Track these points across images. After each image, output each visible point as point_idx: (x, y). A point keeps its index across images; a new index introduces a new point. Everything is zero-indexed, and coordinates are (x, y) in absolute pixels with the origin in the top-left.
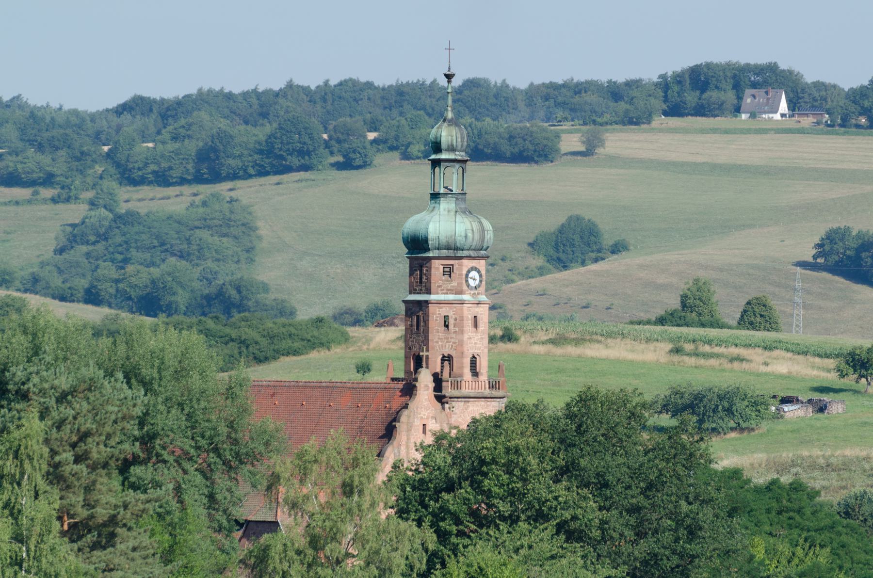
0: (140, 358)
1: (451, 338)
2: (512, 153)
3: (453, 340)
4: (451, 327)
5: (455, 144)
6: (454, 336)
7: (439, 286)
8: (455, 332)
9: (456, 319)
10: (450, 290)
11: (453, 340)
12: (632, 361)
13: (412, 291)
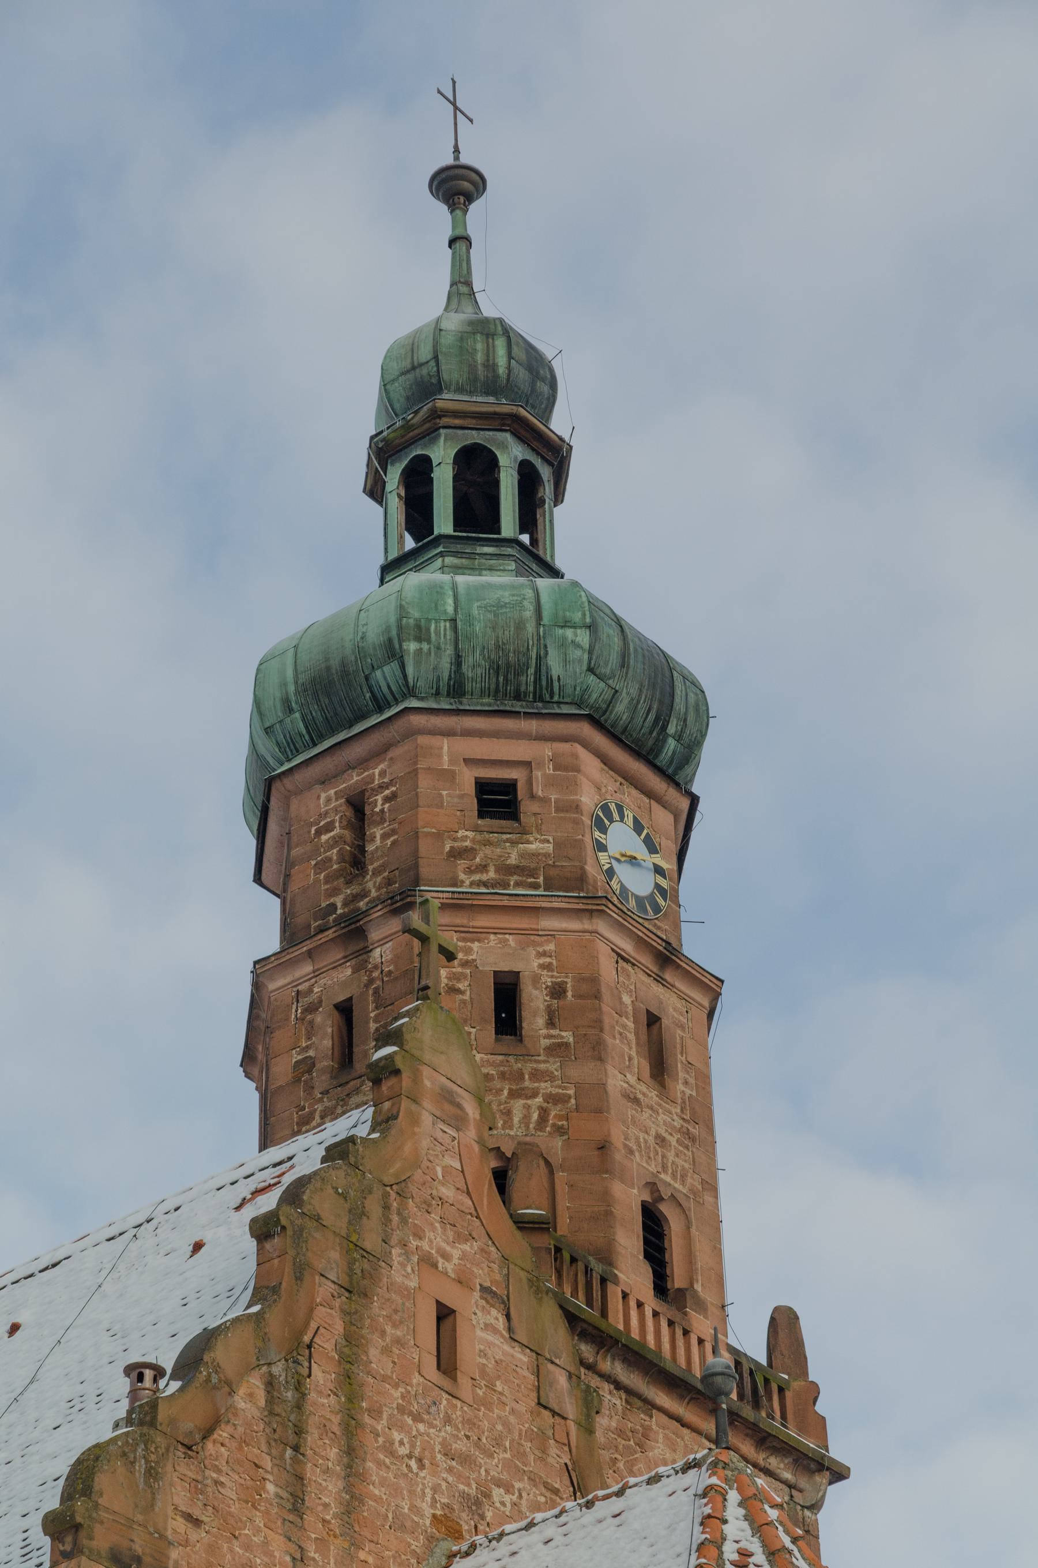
1: (536, 1075)
5: (502, 371)
6: (553, 1066)
7: (456, 854)
8: (558, 1049)
9: (557, 991)
10: (517, 870)
11: (545, 1087)
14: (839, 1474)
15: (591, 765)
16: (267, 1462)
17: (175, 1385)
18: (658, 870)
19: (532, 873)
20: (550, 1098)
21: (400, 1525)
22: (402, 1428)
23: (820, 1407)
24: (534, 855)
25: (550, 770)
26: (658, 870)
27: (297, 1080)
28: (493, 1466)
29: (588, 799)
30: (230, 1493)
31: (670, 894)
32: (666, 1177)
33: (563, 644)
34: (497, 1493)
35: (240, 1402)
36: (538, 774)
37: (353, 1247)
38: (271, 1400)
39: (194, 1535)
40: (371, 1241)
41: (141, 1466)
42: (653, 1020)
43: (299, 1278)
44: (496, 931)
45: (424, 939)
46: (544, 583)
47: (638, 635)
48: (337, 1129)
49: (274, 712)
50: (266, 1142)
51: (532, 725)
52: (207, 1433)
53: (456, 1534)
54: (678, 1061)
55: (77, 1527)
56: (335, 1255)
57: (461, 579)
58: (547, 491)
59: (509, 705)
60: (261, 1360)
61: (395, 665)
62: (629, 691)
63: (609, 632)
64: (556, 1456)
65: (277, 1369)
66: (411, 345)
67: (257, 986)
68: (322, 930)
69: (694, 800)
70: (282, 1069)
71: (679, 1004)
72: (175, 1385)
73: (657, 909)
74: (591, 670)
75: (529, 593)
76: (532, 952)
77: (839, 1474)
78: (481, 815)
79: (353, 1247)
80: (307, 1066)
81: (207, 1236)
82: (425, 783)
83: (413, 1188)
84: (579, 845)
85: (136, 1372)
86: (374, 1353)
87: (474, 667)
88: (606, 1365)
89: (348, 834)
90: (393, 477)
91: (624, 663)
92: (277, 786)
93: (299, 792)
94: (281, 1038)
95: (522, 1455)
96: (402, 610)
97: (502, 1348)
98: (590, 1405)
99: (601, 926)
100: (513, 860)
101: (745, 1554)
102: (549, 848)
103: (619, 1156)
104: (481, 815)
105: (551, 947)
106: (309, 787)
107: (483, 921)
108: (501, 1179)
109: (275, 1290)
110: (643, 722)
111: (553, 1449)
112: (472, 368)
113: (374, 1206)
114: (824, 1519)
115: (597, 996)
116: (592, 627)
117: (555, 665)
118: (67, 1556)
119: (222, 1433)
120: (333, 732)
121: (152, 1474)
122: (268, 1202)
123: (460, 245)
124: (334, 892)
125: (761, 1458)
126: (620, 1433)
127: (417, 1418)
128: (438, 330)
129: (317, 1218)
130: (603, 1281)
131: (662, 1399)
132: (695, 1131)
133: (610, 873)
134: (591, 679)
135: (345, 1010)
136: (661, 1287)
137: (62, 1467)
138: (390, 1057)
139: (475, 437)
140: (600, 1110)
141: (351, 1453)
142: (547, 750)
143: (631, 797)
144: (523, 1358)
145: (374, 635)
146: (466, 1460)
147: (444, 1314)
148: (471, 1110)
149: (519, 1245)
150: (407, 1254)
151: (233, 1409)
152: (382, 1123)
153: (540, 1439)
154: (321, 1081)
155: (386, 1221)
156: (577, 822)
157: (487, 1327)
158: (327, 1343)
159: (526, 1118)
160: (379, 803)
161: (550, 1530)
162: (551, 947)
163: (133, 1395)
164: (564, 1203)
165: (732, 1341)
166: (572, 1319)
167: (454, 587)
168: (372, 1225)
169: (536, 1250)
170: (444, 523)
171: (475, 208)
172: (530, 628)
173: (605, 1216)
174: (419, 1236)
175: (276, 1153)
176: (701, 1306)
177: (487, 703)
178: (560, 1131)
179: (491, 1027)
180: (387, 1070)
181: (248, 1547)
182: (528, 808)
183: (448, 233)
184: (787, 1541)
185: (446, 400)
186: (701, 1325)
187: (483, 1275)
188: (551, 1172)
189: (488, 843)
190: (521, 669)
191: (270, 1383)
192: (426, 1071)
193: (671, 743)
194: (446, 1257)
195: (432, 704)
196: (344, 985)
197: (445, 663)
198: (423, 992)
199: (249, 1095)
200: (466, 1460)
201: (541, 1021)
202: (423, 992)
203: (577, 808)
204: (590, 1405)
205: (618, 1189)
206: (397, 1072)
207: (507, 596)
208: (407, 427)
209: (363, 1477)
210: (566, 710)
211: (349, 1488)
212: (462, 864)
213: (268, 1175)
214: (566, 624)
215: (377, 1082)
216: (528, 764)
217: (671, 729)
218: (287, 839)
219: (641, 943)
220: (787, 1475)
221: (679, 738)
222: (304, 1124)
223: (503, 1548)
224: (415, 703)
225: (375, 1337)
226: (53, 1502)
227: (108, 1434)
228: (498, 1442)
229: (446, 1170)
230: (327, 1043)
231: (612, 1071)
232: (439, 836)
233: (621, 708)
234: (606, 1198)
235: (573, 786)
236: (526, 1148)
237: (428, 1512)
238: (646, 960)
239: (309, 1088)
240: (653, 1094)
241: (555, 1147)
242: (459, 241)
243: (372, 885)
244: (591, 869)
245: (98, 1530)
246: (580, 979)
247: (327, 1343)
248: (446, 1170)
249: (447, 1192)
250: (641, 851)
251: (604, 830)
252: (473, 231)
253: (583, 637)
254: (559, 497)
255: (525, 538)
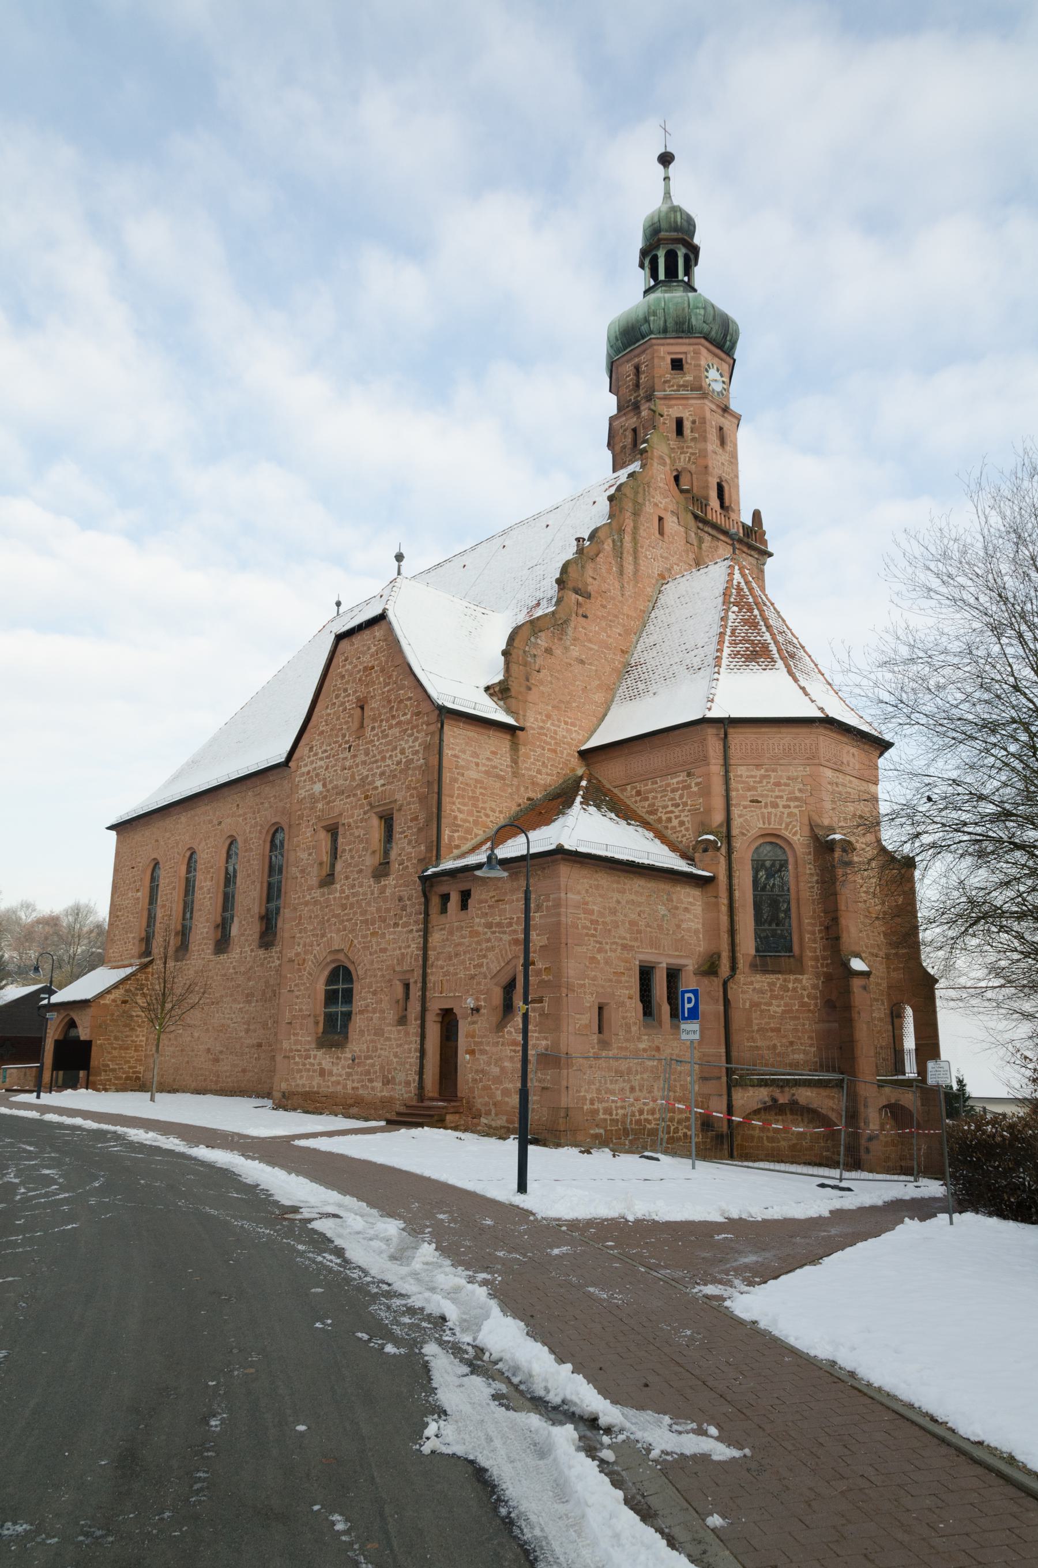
0: (396, 699)
1: (688, 447)
2: (712, 1516)
3: (690, 450)
4: (687, 430)
5: (679, 223)
6: (692, 444)
7: (665, 382)
8: (694, 439)
9: (694, 422)
10: (683, 386)
11: (690, 450)
12: (792, 1163)
13: (678, 1017)
14: (770, 555)
15: (704, 351)
16: (613, 562)
17: (589, 543)
18: (724, 382)
19: (687, 387)
20: (691, 454)
21: (649, 577)
22: (649, 551)
23: (766, 537)
24: (687, 381)
25: (692, 354)
26: (724, 382)
27: (622, 451)
28: (674, 559)
29: (703, 363)
30: (604, 571)
31: (727, 390)
32: (724, 475)
33: (696, 314)
34: (675, 567)
35: (606, 546)
36: (689, 356)
37: (635, 502)
38: (614, 546)
39: (594, 582)
40: (640, 500)
41: (580, 565)
42: (721, 429)
43: (621, 512)
44: (676, 405)
45: (654, 411)
46: (691, 295)
47: (719, 309)
48: (631, 469)
49: (613, 339)
50: (614, 471)
51: (687, 341)
52: (597, 555)
53: (664, 578)
54: (728, 441)
55: (564, 582)
56: (630, 504)
57: (667, 295)
58: (693, 263)
59: (681, 335)
60: (611, 535)
61: (647, 324)
62: (715, 327)
63: (710, 310)
64: (692, 556)
65: (615, 537)
66: (652, 217)
67: (610, 424)
68: (628, 407)
69: (734, 361)
70: (618, 448)
71: (729, 423)
72: (589, 543)
73: (723, 395)
74: (704, 322)
75: (686, 298)
76: (687, 411)
77: (770, 555)
78: (672, 369)
79: (635, 502)
80: (624, 447)
81: (596, 499)
82: (656, 361)
83: (651, 484)
84: (700, 377)
85: (578, 540)
86: (641, 531)
87: (670, 324)
88: (706, 529)
89: (635, 378)
90: (647, 263)
91: (714, 319)
92: (614, 364)
93: (621, 365)
94: (617, 439)
95: (681, 556)
96: (649, 307)
97: (677, 527)
98: (701, 541)
99: (706, 401)
100: (681, 383)
101: (739, 583)
102: (692, 378)
103: (710, 469)
104: (672, 369)
105: (692, 409)
106: (623, 363)
107: (673, 402)
108: (677, 479)
109: (614, 515)
110: (720, 337)
111: (690, 554)
112: (670, 223)
113: (641, 490)
114: (766, 568)
115: (705, 423)
116: (705, 308)
117: (694, 321)
118: (562, 589)
119: (601, 555)
120: (630, 346)
121: (583, 567)
122: (612, 491)
123: (667, 180)
124: (631, 395)
125: (749, 552)
126: (710, 547)
127: (653, 548)
128: (660, 211)
129: (625, 495)
130: (706, 505)
131: (722, 537)
132: (732, 460)
133: (709, 385)
134: (705, 325)
135: (635, 430)
136: (722, 506)
137: (561, 565)
138: (645, 447)
139: (671, 247)
140: (705, 456)
141: (636, 558)
142: (691, 348)
143: (716, 360)
144: (682, 529)
145: (641, 315)
146: (666, 558)
147: (661, 519)
148: (668, 461)
149: (681, 497)
150: (650, 503)
151: (603, 548)
152: (643, 466)
153: (687, 552)
154: (628, 451)
155: (644, 494)
156: (700, 370)
157: (673, 522)
158: (629, 530)
159: (685, 460)
160: (643, 368)
161: (688, 577)
162: (692, 409)
163: (578, 546)
164: (695, 484)
165: (742, 520)
166: (696, 517)
167: (664, 298)
168: (640, 495)
169: (686, 498)
170: (662, 276)
171: (672, 166)
172: (686, 309)
173: (706, 487)
174: (653, 498)
175: (616, 475)
176: (733, 511)
177: (674, 335)
178: (694, 463)
179: (675, 434)
180: (645, 451)
181: (609, 584)
182: (686, 366)
183: (663, 176)
184: (751, 579)
185: (663, 235)
186: (733, 516)
187: (671, 507)
188: (692, 475)
189: (674, 378)
190: (684, 323)
191: (613, 541)
192: (655, 450)
193: (728, 343)
194: (661, 503)
195: (658, 336)
196: (634, 423)
197: (662, 323)
198: (654, 427)
199: (609, 455)
200: (666, 558)
201: (689, 431)
202: (654, 427)
203: (700, 366)
204: (701, 541)
205: (710, 479)
206: (647, 451)
207: (680, 300)
208: (651, 245)
209: (639, 564)
210: (697, 335)
211: (635, 568)
212: (667, 385)
213: (613, 482)
214: (697, 308)
215: (642, 454)
216: (686, 353)
217: (728, 338)
218: (618, 380)
219: (718, 406)
220: (756, 556)
221: (730, 341)
222: (622, 468)
223: (676, 582)
224: (653, 336)
225: (641, 527)
226: (558, 576)
227: (572, 557)
228: (676, 553)
229: (661, 478)
230: (630, 440)
231: (709, 444)
232: (660, 377)
233: (713, 333)
234: (707, 481)
235: (699, 359)
236: (684, 469)
237: (656, 573)
238: (720, 411)
239: (625, 453)
240: (721, 451)
241: (693, 468)
242: (667, 179)
243: (642, 392)
244: (703, 384)
245: (569, 582)
246: (700, 418)
247: (629, 530)
248: (661, 478)
249: (661, 485)
250: (718, 377)
251: (707, 371)
252: (670, 175)
253: (702, 312)
254: (696, 264)
255: (686, 279)
